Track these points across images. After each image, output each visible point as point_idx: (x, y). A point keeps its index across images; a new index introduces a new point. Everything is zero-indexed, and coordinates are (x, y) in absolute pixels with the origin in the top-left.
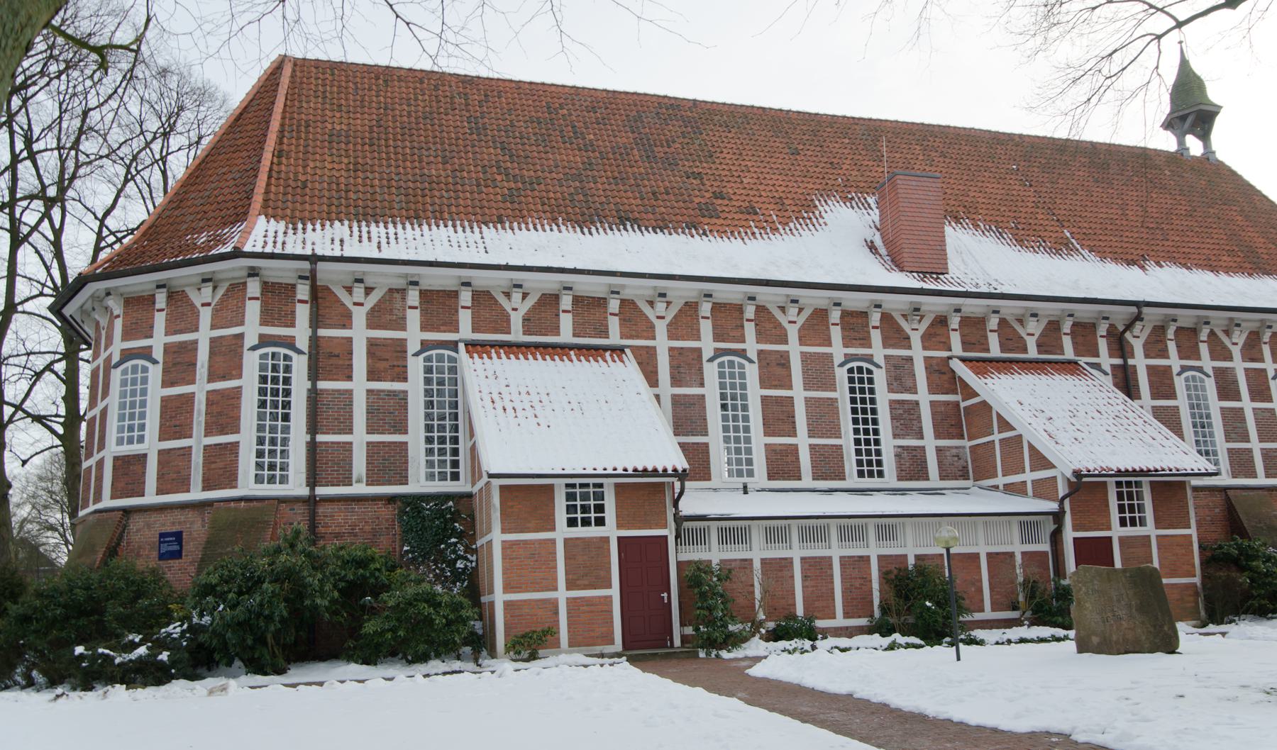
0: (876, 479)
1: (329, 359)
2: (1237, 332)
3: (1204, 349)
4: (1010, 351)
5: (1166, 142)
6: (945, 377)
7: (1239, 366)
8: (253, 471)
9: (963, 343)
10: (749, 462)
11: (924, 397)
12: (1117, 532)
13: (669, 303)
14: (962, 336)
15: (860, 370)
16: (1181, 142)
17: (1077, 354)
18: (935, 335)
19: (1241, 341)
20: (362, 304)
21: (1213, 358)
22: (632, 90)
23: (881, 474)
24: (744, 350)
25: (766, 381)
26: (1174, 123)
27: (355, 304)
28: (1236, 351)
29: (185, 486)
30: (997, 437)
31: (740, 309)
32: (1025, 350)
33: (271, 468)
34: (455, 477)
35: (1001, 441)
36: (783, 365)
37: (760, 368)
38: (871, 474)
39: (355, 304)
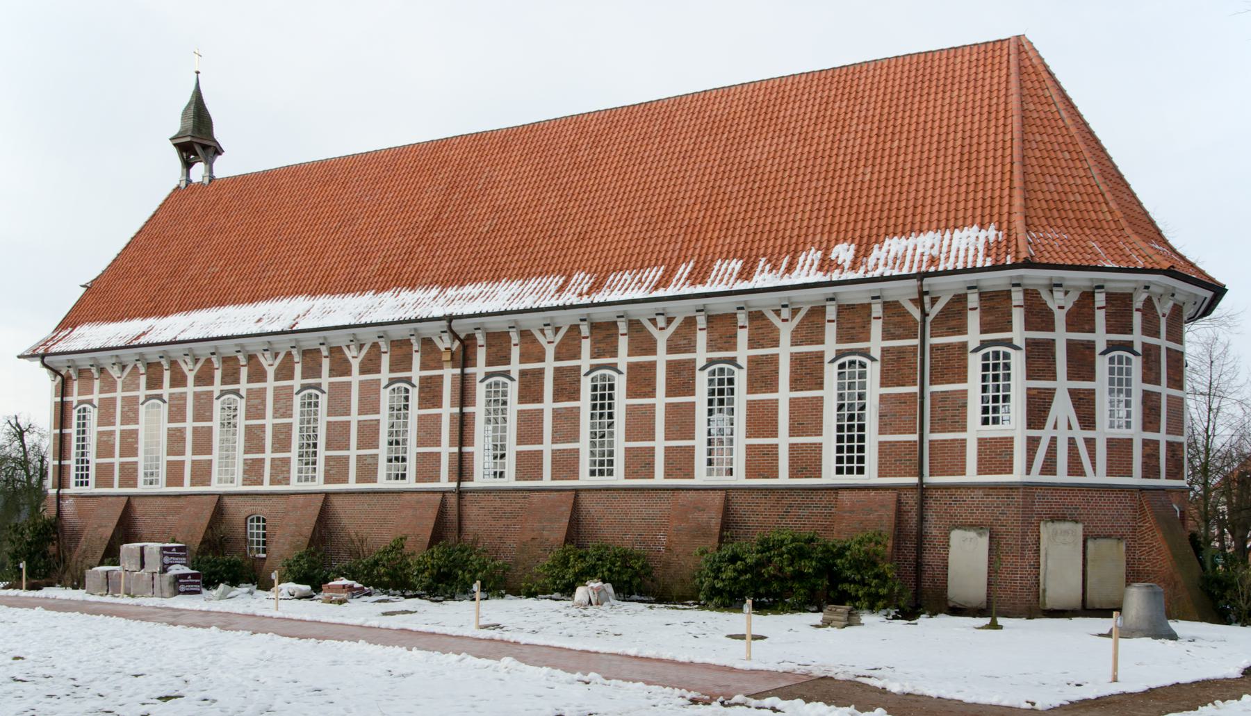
1: (763, 375)
8: (834, 465)
13: (1066, 293)
22: (1086, 118)
24: (868, 349)
25: (423, 403)
29: (436, 478)
31: (867, 307)
33: (603, 466)
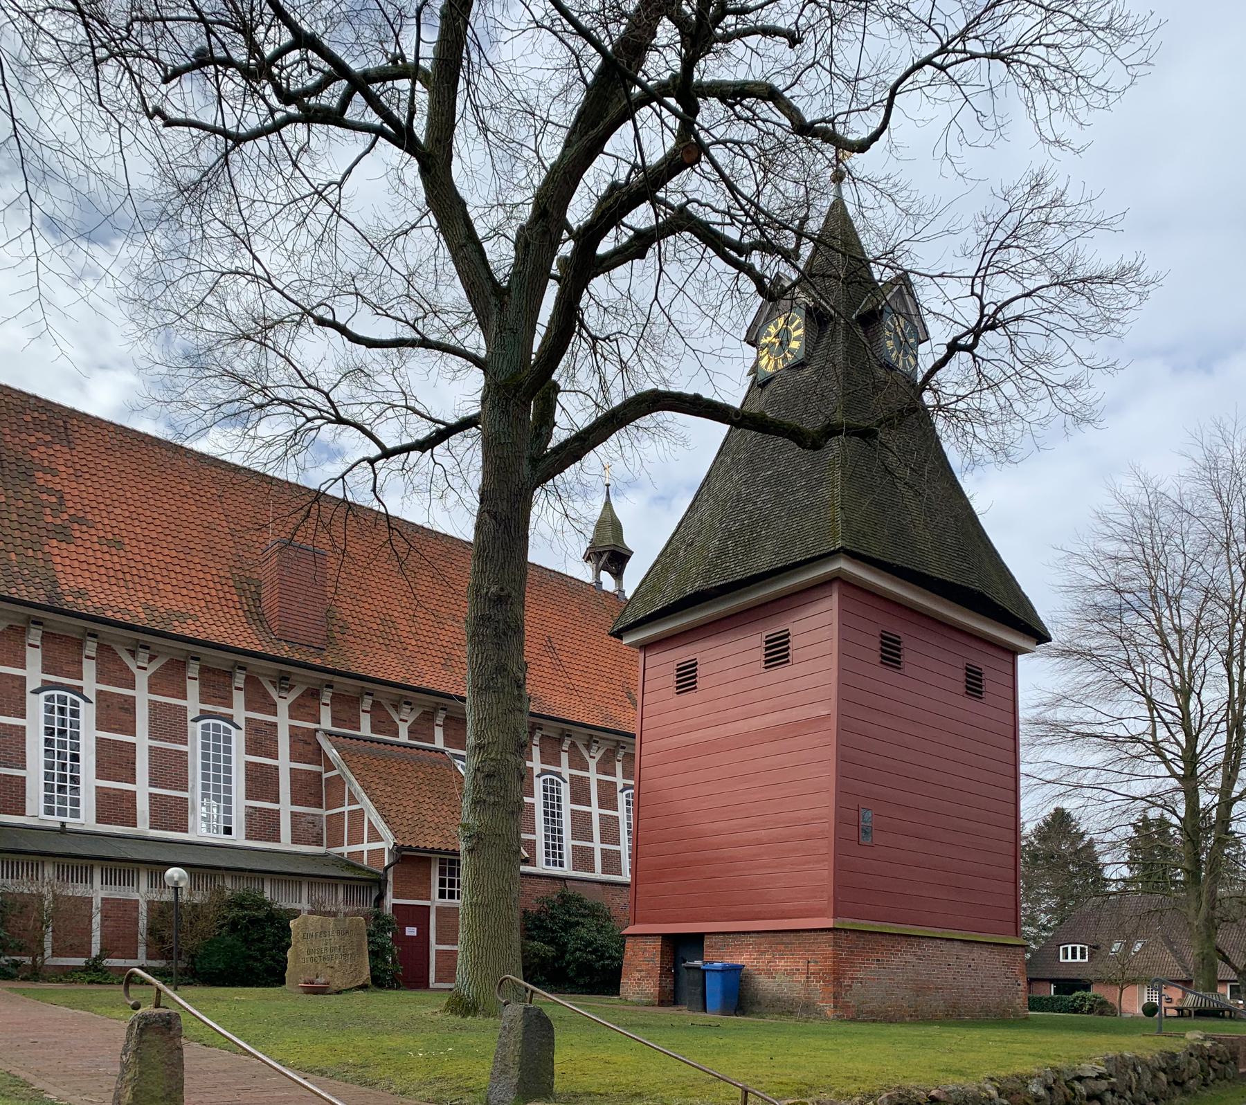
0: (558, 868)
2: (595, 747)
3: (564, 758)
4: (381, 732)
5: (584, 572)
6: (311, 748)
7: (593, 776)
9: (333, 718)
10: (561, 856)
11: (284, 763)
12: (435, 901)
14: (333, 711)
15: (552, 780)
16: (597, 576)
17: (447, 744)
18: (304, 706)
19: (598, 756)
20: (145, 669)
21: (249, 707)
23: (561, 865)
25: (253, 747)
26: (593, 555)
27: (139, 667)
28: (593, 764)
30: (346, 809)
32: (397, 735)
34: (561, 865)
35: (349, 812)
36: (127, 710)
37: (97, 708)
38: (555, 864)
39: (139, 667)
